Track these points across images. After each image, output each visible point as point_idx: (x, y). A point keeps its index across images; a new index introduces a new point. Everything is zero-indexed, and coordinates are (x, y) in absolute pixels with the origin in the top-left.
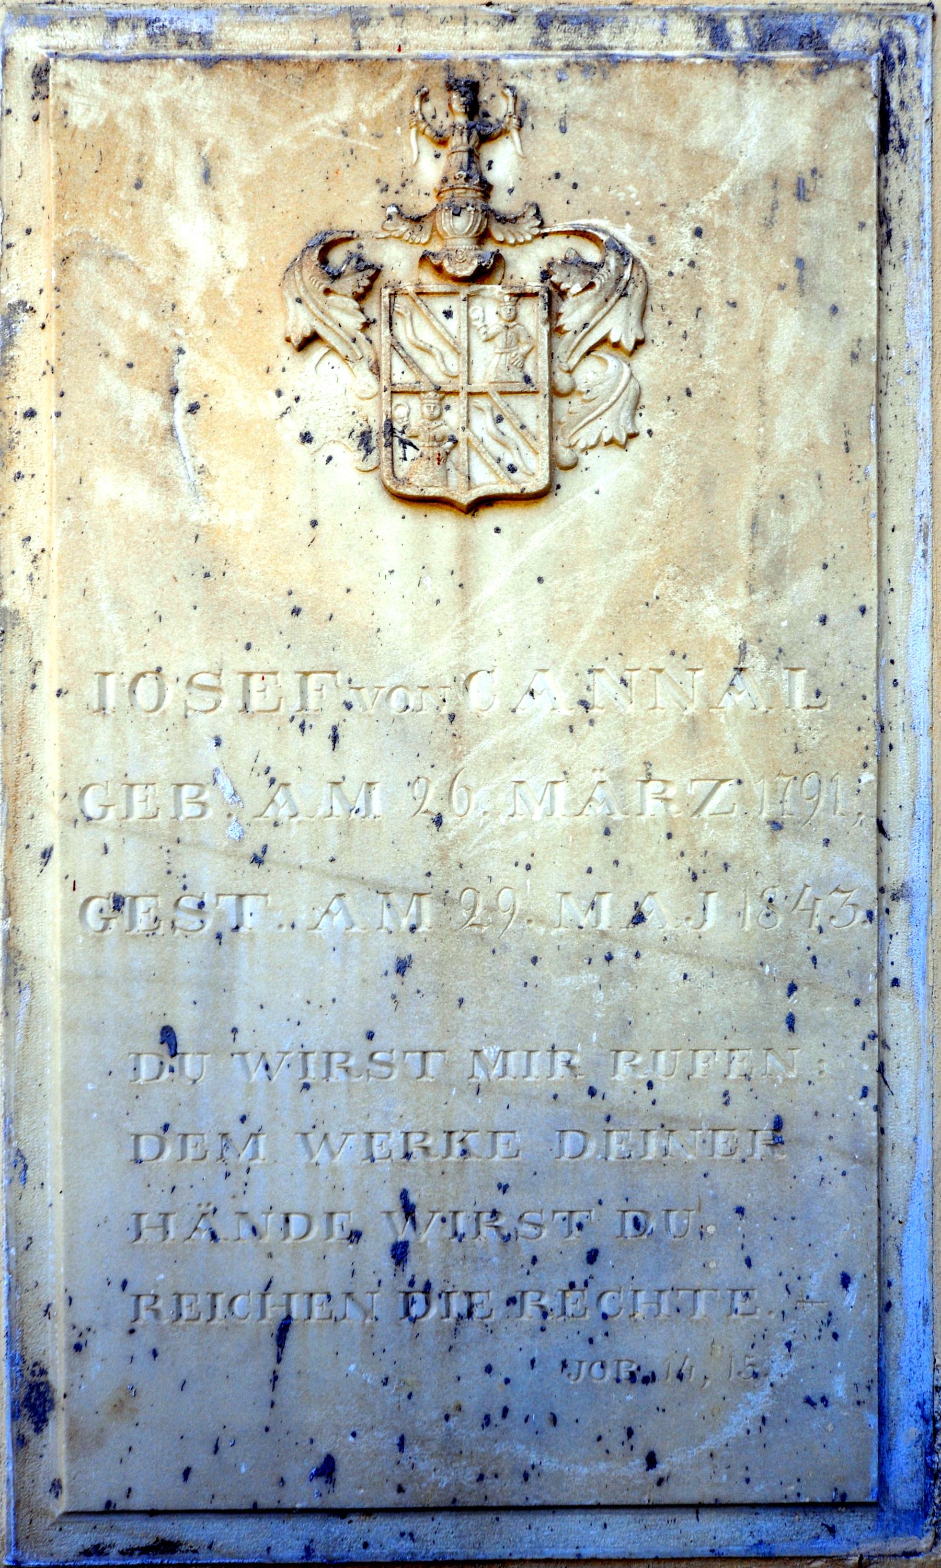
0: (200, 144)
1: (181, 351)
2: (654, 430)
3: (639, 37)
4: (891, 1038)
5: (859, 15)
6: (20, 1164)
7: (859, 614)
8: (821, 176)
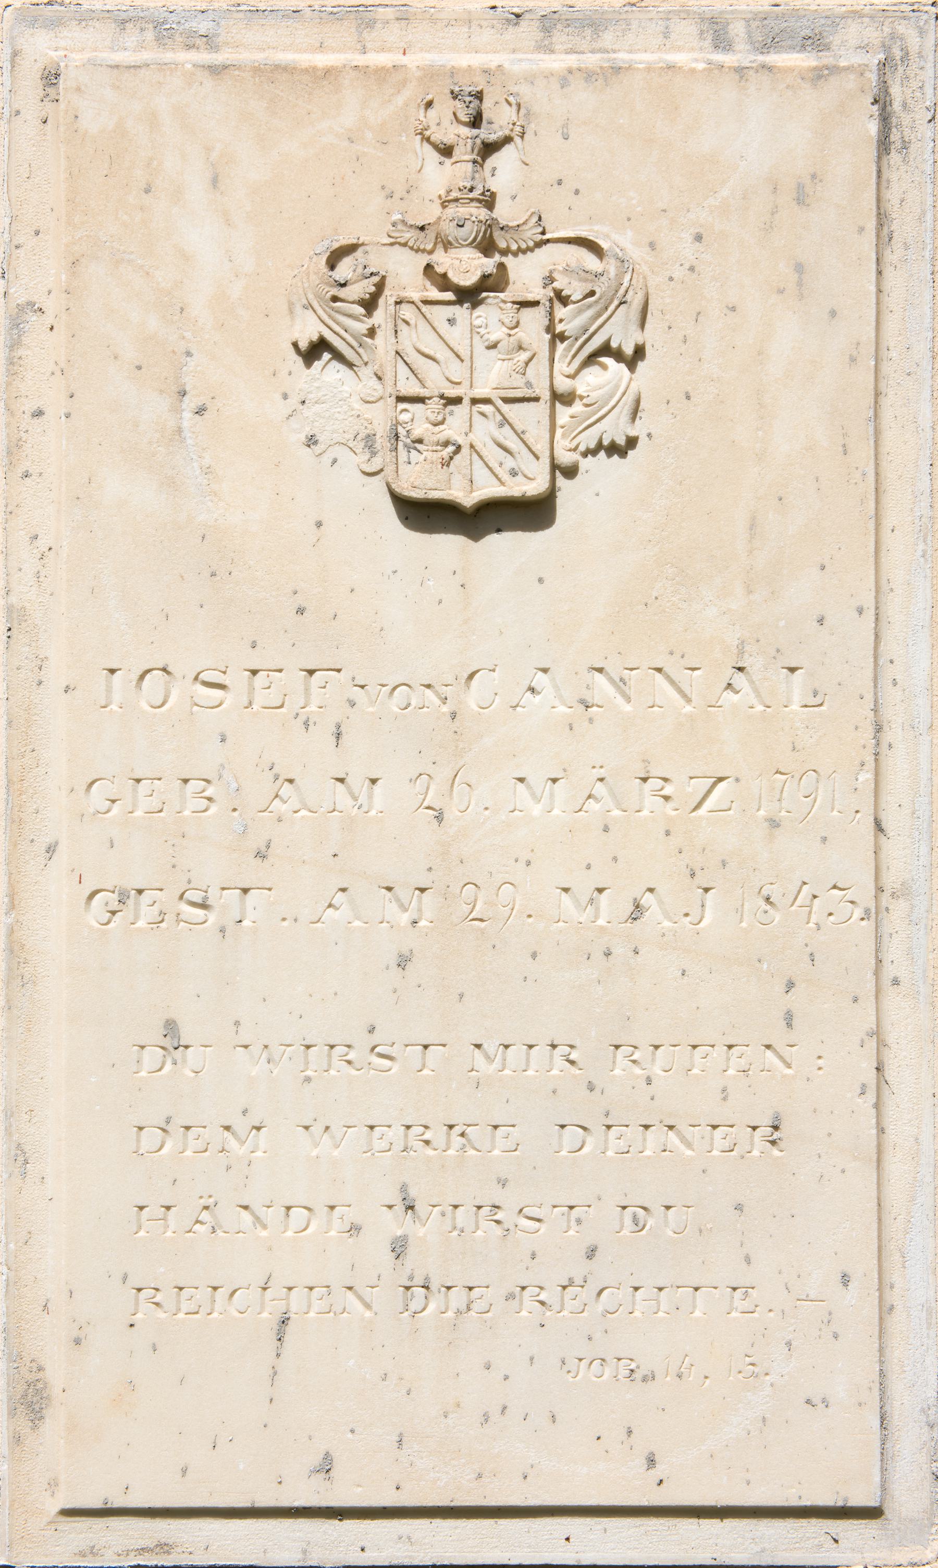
0: (208, 149)
1: (189, 354)
2: (653, 433)
3: (639, 50)
4: (891, 1039)
5: (861, 16)
6: (21, 1158)
7: (856, 614)
8: (821, 181)
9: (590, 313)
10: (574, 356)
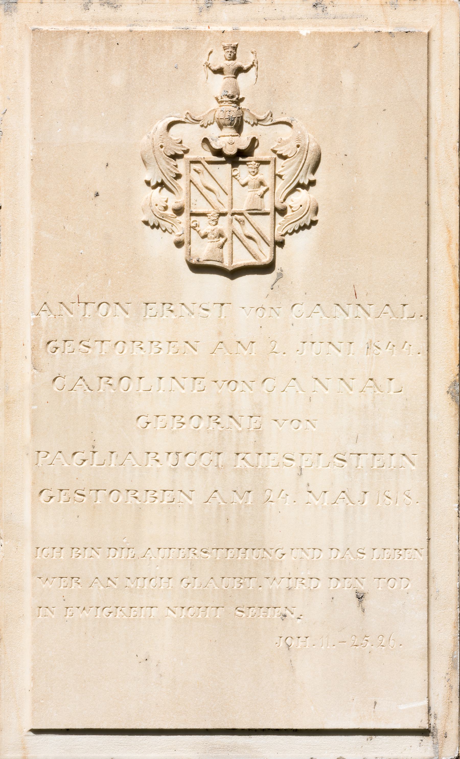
9: (296, 164)
10: (287, 188)
